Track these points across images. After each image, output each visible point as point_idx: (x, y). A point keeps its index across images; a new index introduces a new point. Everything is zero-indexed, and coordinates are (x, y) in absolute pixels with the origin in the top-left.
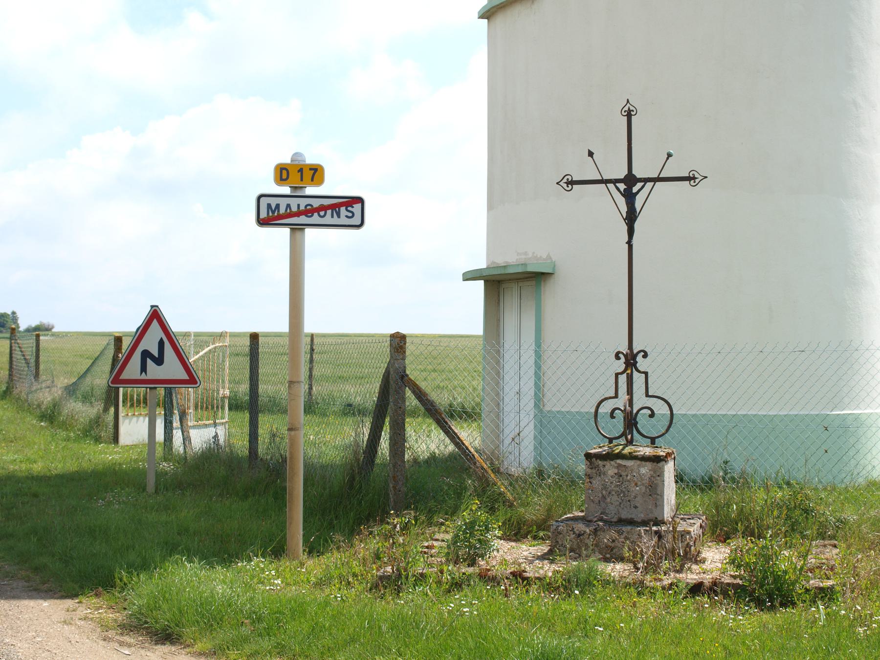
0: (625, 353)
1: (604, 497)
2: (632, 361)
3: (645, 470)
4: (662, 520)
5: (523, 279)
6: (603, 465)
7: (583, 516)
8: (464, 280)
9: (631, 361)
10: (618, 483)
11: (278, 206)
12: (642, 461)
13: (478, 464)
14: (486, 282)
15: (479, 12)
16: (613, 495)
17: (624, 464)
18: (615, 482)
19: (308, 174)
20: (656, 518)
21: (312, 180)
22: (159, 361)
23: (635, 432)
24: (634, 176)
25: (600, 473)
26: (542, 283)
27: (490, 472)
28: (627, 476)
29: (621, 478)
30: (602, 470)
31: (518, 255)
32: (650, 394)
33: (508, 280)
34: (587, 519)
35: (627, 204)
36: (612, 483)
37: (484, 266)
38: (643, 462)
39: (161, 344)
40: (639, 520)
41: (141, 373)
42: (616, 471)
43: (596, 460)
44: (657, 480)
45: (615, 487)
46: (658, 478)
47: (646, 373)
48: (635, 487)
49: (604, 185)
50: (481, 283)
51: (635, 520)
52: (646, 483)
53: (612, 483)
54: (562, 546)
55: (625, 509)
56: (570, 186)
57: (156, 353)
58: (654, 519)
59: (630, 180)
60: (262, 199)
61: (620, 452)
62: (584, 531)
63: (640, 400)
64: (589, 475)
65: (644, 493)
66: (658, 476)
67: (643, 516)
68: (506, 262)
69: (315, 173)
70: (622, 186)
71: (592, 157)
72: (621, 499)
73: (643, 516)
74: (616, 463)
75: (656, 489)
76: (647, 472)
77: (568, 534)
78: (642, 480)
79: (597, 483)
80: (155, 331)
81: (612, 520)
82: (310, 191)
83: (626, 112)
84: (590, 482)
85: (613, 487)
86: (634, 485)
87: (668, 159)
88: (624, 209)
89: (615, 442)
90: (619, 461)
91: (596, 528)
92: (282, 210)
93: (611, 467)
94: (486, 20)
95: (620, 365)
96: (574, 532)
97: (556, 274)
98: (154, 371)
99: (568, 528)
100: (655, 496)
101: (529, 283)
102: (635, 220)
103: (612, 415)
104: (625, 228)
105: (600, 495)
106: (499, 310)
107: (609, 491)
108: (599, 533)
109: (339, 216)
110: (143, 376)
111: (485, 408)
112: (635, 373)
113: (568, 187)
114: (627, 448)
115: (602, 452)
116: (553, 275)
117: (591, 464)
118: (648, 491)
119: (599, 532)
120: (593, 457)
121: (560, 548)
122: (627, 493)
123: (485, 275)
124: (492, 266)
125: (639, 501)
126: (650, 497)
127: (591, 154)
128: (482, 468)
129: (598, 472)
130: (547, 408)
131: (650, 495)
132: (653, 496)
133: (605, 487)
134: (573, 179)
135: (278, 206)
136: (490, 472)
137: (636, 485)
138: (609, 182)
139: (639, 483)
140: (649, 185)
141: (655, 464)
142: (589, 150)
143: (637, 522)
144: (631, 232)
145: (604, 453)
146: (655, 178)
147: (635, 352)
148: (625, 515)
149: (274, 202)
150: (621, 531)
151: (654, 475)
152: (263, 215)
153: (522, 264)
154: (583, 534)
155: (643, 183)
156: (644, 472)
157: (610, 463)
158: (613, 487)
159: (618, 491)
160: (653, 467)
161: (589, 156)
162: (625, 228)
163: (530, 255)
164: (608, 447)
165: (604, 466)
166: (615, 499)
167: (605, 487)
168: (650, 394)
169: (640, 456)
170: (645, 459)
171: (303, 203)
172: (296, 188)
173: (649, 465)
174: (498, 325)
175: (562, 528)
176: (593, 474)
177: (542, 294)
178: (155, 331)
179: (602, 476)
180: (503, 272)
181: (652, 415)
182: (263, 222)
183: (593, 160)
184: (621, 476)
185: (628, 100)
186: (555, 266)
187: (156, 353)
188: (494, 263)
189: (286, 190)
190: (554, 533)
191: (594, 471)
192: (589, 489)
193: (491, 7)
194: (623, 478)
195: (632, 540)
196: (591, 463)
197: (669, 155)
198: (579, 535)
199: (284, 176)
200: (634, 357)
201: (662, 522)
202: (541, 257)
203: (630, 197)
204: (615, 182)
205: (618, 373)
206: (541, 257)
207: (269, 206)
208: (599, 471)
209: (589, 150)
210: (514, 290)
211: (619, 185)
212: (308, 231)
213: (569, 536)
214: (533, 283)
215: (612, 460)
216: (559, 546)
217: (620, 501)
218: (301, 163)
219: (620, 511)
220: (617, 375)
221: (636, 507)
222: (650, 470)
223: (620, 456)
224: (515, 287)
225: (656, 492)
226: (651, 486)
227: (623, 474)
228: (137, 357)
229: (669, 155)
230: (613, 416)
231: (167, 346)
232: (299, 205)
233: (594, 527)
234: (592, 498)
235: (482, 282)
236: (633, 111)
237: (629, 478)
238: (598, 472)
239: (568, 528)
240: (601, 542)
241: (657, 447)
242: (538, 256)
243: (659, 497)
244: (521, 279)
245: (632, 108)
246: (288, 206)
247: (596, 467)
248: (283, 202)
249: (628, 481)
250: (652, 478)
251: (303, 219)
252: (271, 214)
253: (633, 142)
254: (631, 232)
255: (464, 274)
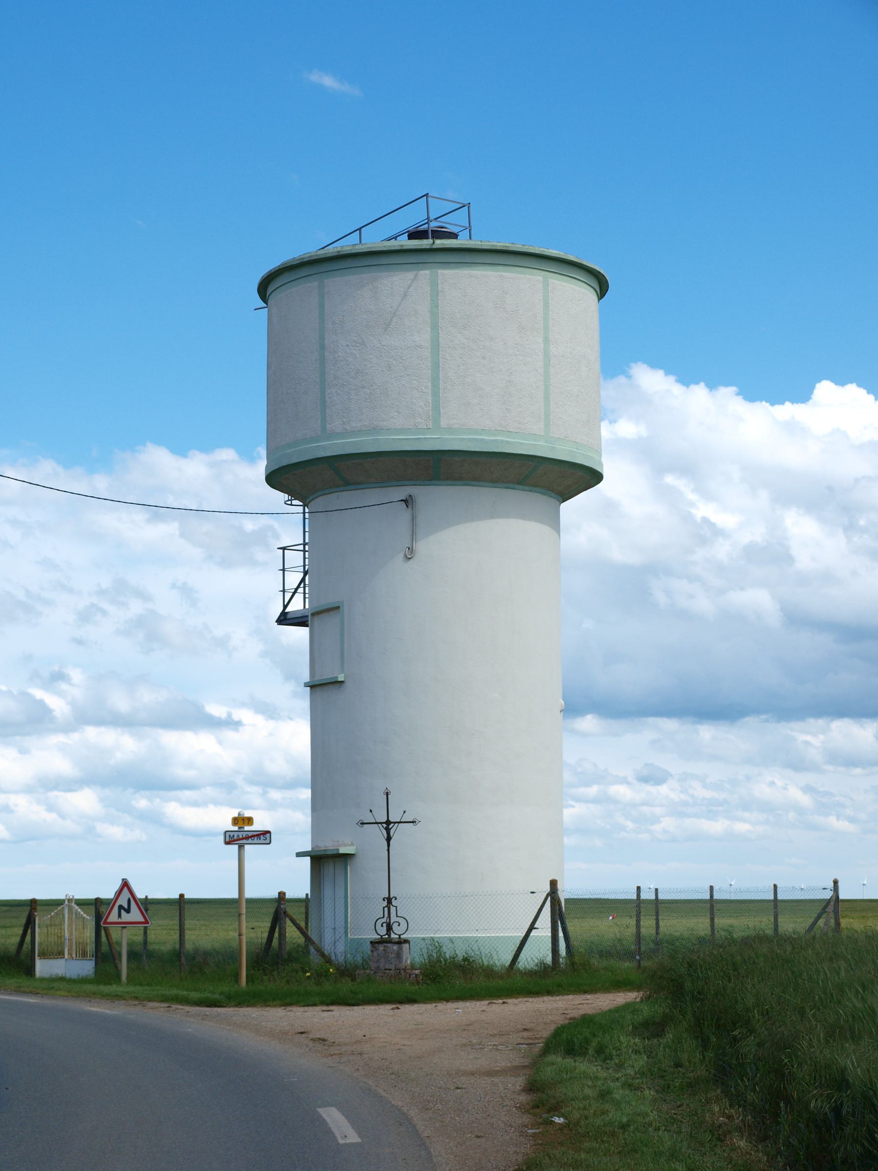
1: (378, 960)
3: (395, 947)
9: (389, 900)
11: (233, 836)
19: (246, 822)
21: (248, 823)
22: (128, 911)
23: (392, 932)
37: (310, 849)
39: (129, 901)
41: (118, 919)
57: (126, 907)
59: (388, 822)
60: (227, 833)
63: (393, 918)
68: (326, 847)
69: (250, 821)
70: (385, 825)
79: (375, 954)
80: (126, 894)
82: (247, 828)
88: (386, 836)
90: (385, 944)
92: (235, 838)
95: (385, 903)
98: (126, 917)
103: (382, 926)
109: (260, 839)
110: (120, 920)
112: (391, 906)
127: (371, 811)
135: (233, 836)
137: (392, 954)
140: (397, 824)
144: (389, 845)
149: (232, 834)
152: (227, 840)
162: (386, 843)
167: (378, 955)
171: (244, 834)
172: (241, 827)
178: (126, 894)
182: (227, 843)
187: (126, 907)
188: (317, 846)
189: (236, 828)
197: (404, 812)
199: (236, 822)
203: (388, 830)
204: (381, 823)
207: (230, 836)
211: (383, 825)
212: (246, 846)
218: (243, 816)
220: (384, 908)
221: (392, 963)
227: (386, 949)
228: (116, 909)
229: (404, 812)
231: (133, 902)
232: (243, 835)
246: (238, 836)
248: (236, 834)
251: (244, 841)
252: (230, 839)
254: (389, 845)
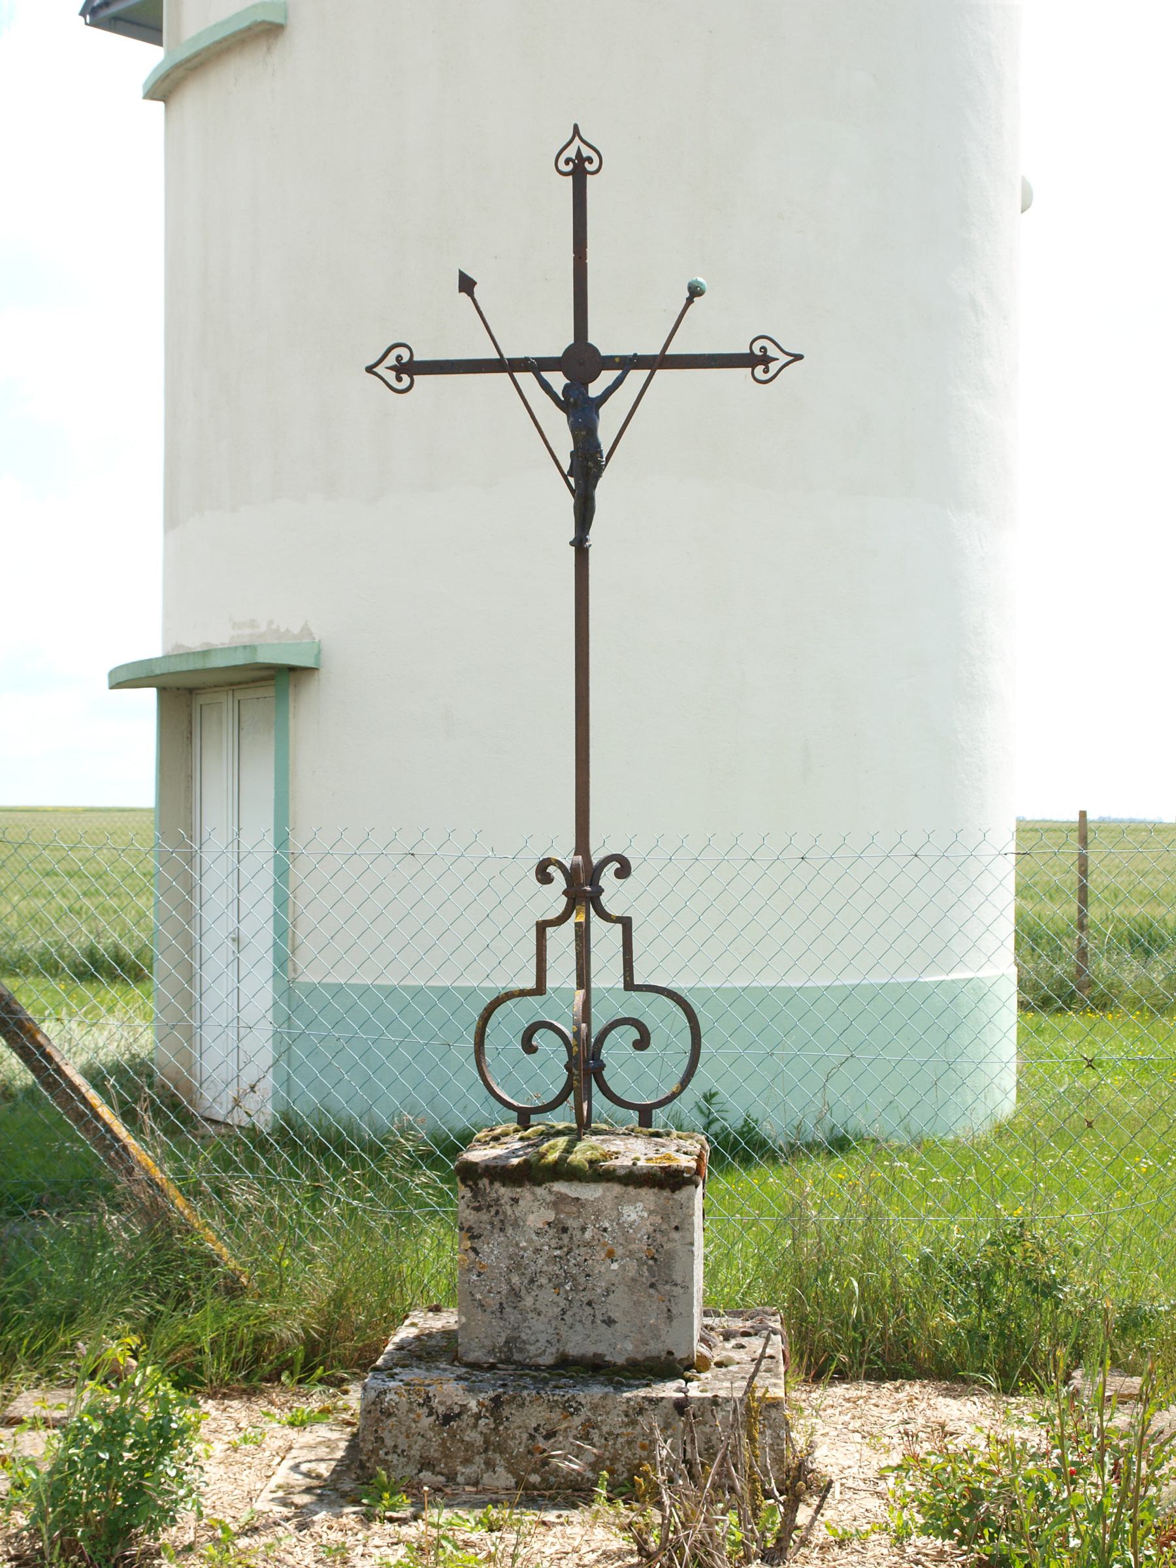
0: (568, 866)
1: (515, 1293)
2: (588, 888)
4: (687, 1359)
5: (247, 683)
6: (512, 1199)
7: (448, 1334)
8: (111, 688)
10: (557, 1252)
12: (626, 1185)
13: (138, 1174)
14: (163, 691)
15: (145, 85)
16: (542, 1285)
17: (574, 1195)
18: (546, 1248)
20: (670, 1353)
24: (595, 350)
25: (502, 1221)
26: (291, 690)
27: (172, 1192)
28: (583, 1229)
29: (565, 1237)
30: (509, 1212)
31: (233, 628)
32: (638, 980)
33: (210, 687)
34: (465, 1358)
35: (574, 428)
36: (537, 1251)
37: (158, 653)
38: (631, 1189)
40: (620, 1360)
42: (551, 1216)
43: (491, 1183)
44: (674, 1240)
45: (547, 1263)
46: (675, 1235)
47: (626, 923)
48: (609, 1261)
49: (506, 376)
50: (151, 694)
51: (607, 1358)
52: (640, 1250)
53: (537, 1251)
54: (395, 1452)
55: (578, 1326)
56: (405, 377)
58: (664, 1354)
61: (561, 1160)
62: (461, 1406)
64: (470, 1229)
65: (633, 1280)
66: (677, 1228)
67: (630, 1347)
70: (558, 381)
71: (471, 294)
72: (566, 1299)
73: (630, 1347)
74: (550, 1192)
75: (668, 1266)
76: (642, 1218)
77: (412, 1416)
78: (629, 1240)
79: (493, 1251)
81: (541, 1361)
83: (571, 164)
84: (474, 1250)
85: (540, 1261)
86: (603, 1255)
87: (690, 301)
88: (564, 444)
89: (538, 1124)
90: (560, 1187)
91: (498, 1397)
93: (537, 1203)
94: (162, 104)
95: (553, 899)
96: (431, 1408)
97: (321, 669)
99: (414, 1397)
100: (668, 1287)
101: (260, 693)
102: (598, 476)
104: (568, 502)
105: (504, 1288)
106: (189, 755)
107: (528, 1277)
108: (506, 1411)
111: (164, 963)
112: (595, 919)
113: (399, 379)
114: (580, 1146)
115: (507, 1157)
116: (316, 673)
117: (475, 1196)
118: (647, 1274)
119: (506, 1408)
120: (481, 1177)
121: (389, 1458)
122: (582, 1280)
123: (158, 672)
124: (175, 653)
125: (619, 1304)
126: (652, 1291)
128: (152, 1183)
129: (496, 1221)
130: (310, 977)
131: (652, 1286)
132: (659, 1287)
133: (517, 1265)
134: (415, 359)
136: (172, 1192)
137: (610, 1255)
138: (522, 365)
139: (619, 1251)
140: (636, 377)
141: (666, 1193)
142: (460, 272)
143: (615, 1365)
145: (515, 1161)
146: (655, 357)
147: (595, 860)
148: (578, 1344)
150: (575, 1405)
151: (664, 1227)
153: (245, 647)
154: (459, 1415)
155: (619, 372)
156: (634, 1216)
157: (533, 1193)
158: (540, 1261)
159: (557, 1276)
160: (662, 1201)
161: (460, 291)
163: (263, 628)
164: (521, 1139)
165: (515, 1201)
166: (546, 1298)
167: (517, 1265)
168: (638, 980)
169: (622, 1172)
170: (635, 1179)
173: (648, 1195)
174: (189, 789)
175: (395, 1397)
176: (483, 1226)
177: (291, 716)
179: (510, 1231)
180: (199, 664)
181: (642, 1043)
183: (474, 300)
184: (565, 1230)
185: (576, 128)
186: (319, 652)
190: (369, 1412)
191: (485, 1216)
192: (469, 1270)
193: (173, 64)
194: (571, 1238)
195: (605, 1429)
196: (476, 1192)
197: (695, 291)
198: (447, 1419)
200: (594, 873)
201: (686, 1363)
202: (287, 630)
204: (537, 366)
205: (544, 922)
206: (287, 630)
208: (502, 1217)
209: (460, 272)
210: (225, 708)
213: (415, 1421)
214: (271, 692)
215: (540, 1185)
216: (387, 1454)
217: (563, 1303)
219: (564, 1334)
221: (610, 1322)
222: (651, 1213)
223: (562, 1171)
224: (227, 702)
225: (670, 1276)
226: (653, 1258)
227: (572, 1223)
229: (695, 291)
230: (531, 1046)
233: (492, 1394)
234: (478, 1296)
235: (153, 692)
236: (590, 160)
237: (588, 1235)
238: (496, 1221)
239: (414, 1397)
240: (514, 1438)
241: (657, 1135)
242: (282, 630)
243: (678, 1291)
244: (240, 683)
245: (586, 152)
247: (490, 1206)
249: (587, 1244)
250: (658, 1235)
253: (589, 251)
255: (112, 674)
